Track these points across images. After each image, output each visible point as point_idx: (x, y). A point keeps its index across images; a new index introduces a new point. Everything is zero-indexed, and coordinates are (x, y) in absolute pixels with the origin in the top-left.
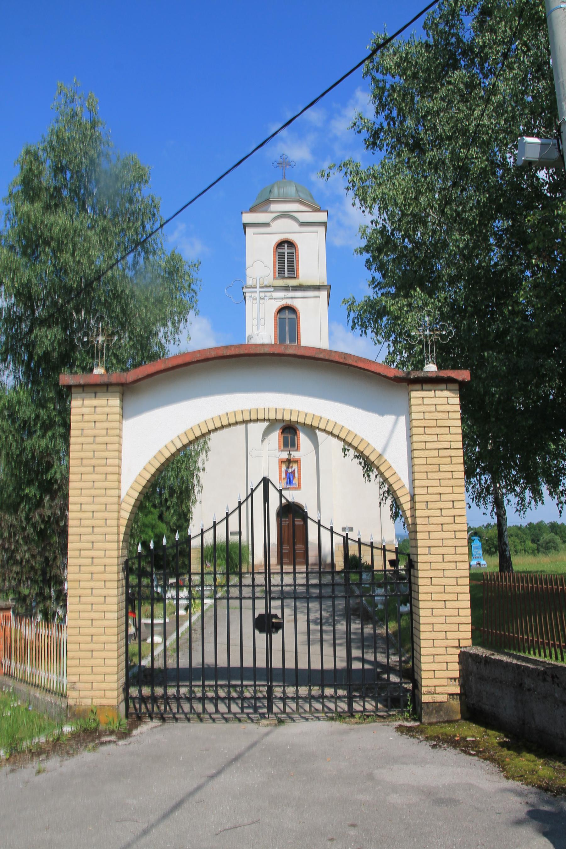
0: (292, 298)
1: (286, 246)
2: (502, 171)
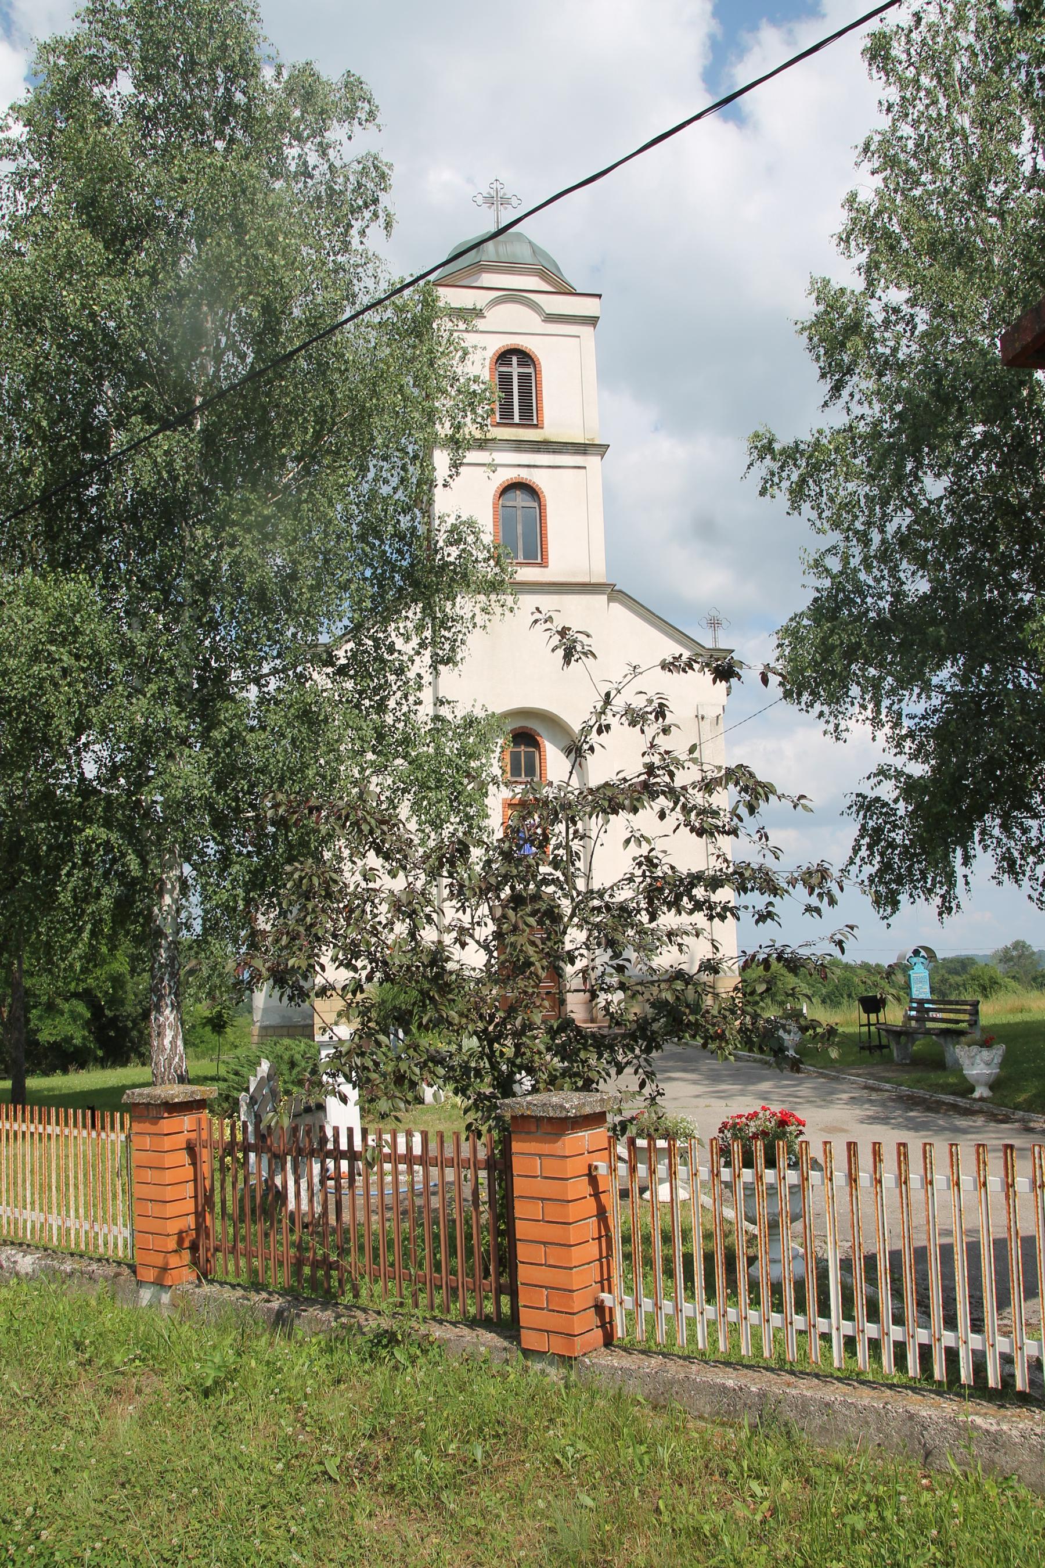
0: (528, 466)
1: (515, 359)
2: (509, 1042)
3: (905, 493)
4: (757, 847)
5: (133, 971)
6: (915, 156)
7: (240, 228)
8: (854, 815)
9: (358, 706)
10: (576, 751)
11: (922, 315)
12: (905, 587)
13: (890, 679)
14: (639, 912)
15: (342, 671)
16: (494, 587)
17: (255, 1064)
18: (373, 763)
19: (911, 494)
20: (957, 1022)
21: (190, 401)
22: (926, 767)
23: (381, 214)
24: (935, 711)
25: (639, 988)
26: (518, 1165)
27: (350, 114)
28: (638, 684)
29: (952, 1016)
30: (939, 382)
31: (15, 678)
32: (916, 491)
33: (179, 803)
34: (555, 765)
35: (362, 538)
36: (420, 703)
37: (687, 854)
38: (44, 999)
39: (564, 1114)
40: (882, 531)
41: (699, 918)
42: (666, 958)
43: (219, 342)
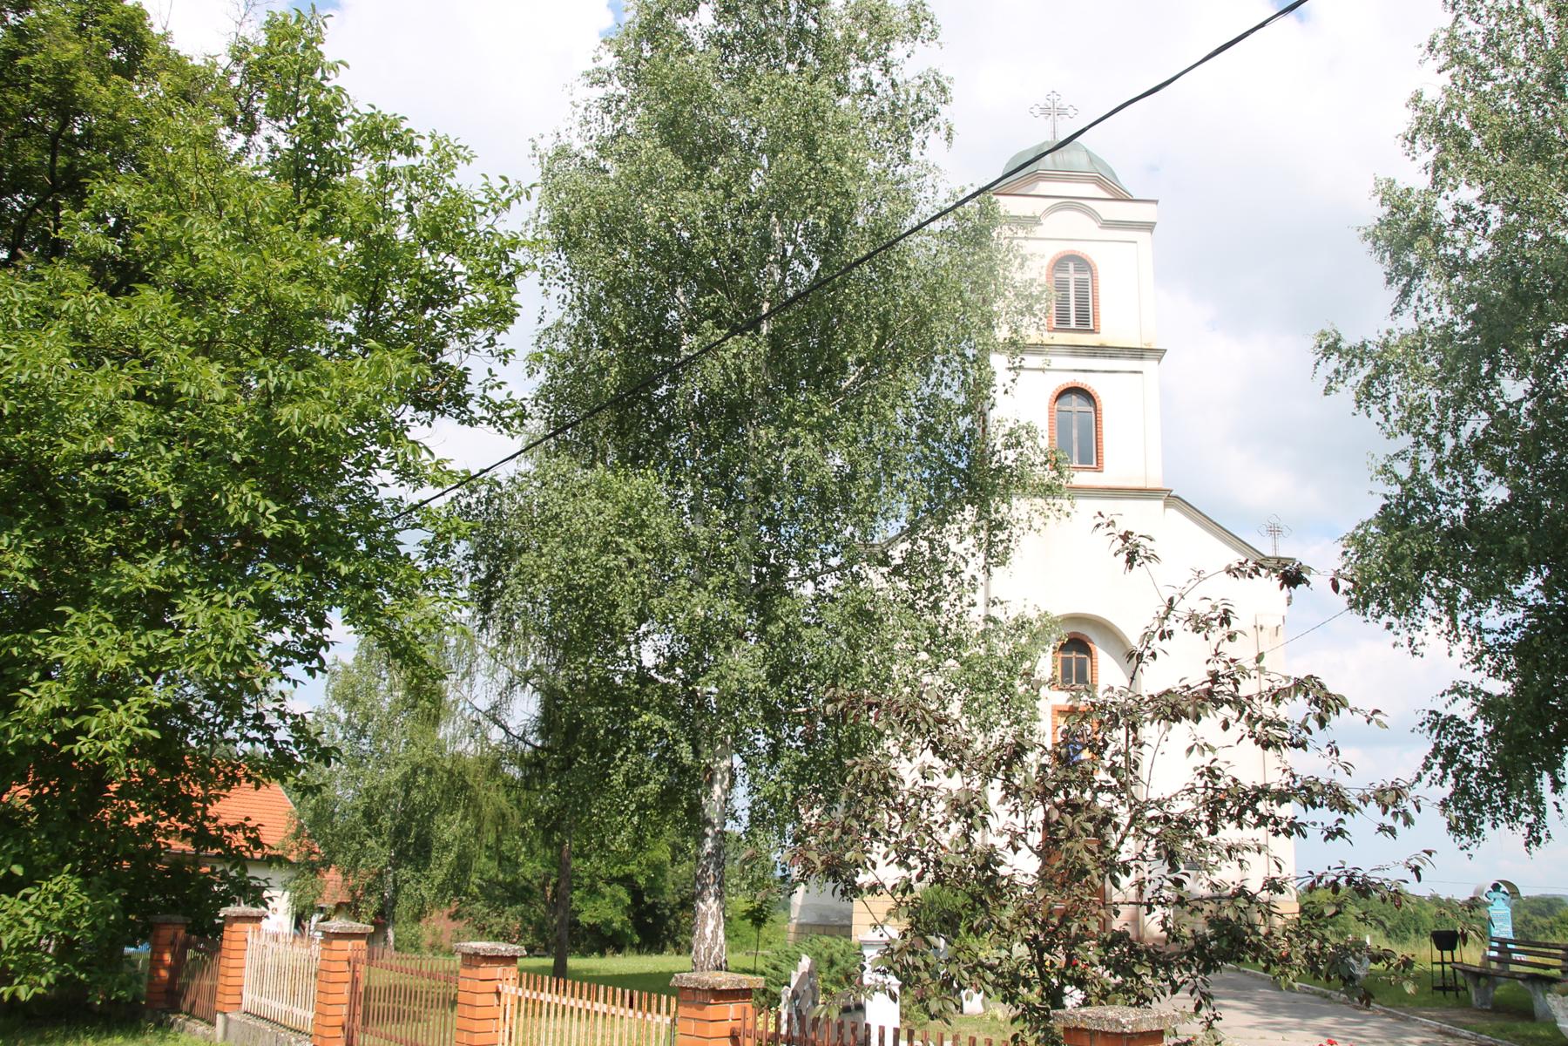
1: (1071, 266)
3: (1480, 396)
4: (1328, 761)
5: (674, 859)
6: (1484, 51)
7: (811, 145)
8: (1427, 733)
9: (912, 606)
10: (1134, 658)
11: (1495, 212)
12: (1481, 495)
13: (1464, 590)
14: (1198, 823)
15: (897, 571)
16: (1049, 490)
17: (794, 960)
18: (924, 663)
19: (1487, 396)
20: (1547, 967)
21: (758, 308)
22: (1508, 684)
23: (942, 126)
24: (1515, 626)
25: (1197, 903)
27: (914, 34)
28: (1203, 589)
29: (1538, 960)
30: (1516, 280)
31: (584, 568)
32: (1492, 393)
33: (734, 695)
34: (1108, 673)
35: (922, 439)
36: (974, 605)
37: (1250, 766)
38: (587, 881)
39: (1119, 1030)
40: (1455, 436)
41: (1262, 834)
42: (1228, 874)
43: (785, 251)
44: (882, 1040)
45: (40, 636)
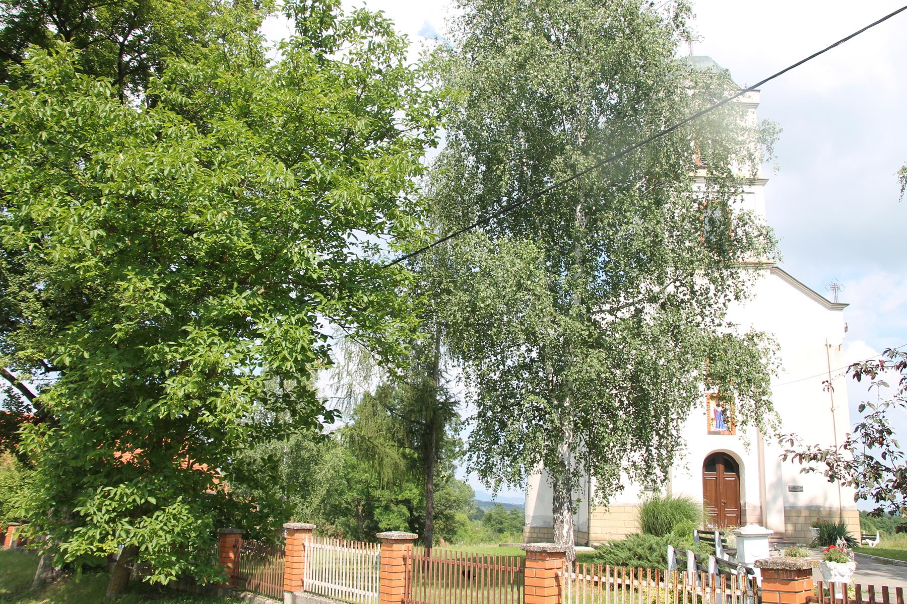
26: (527, 572)
38: (384, 503)
44: (690, 601)
45: (169, 346)
